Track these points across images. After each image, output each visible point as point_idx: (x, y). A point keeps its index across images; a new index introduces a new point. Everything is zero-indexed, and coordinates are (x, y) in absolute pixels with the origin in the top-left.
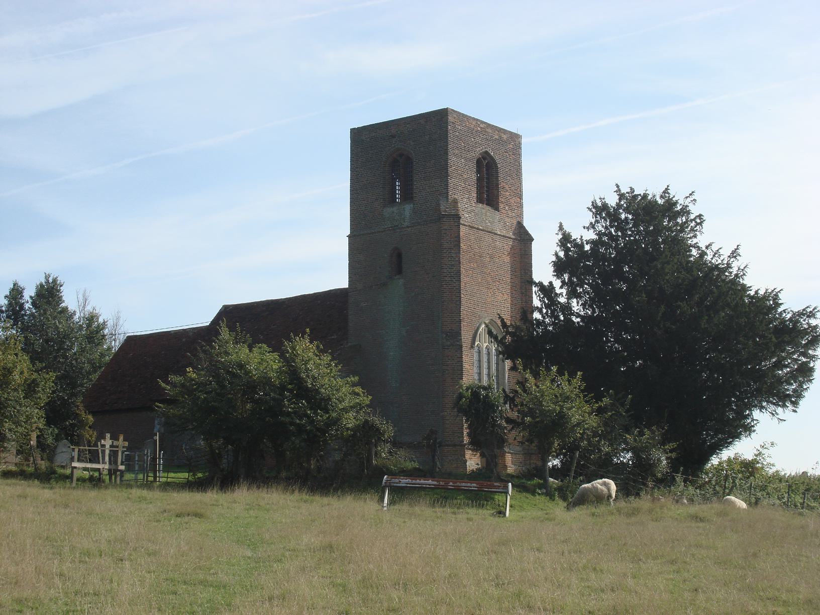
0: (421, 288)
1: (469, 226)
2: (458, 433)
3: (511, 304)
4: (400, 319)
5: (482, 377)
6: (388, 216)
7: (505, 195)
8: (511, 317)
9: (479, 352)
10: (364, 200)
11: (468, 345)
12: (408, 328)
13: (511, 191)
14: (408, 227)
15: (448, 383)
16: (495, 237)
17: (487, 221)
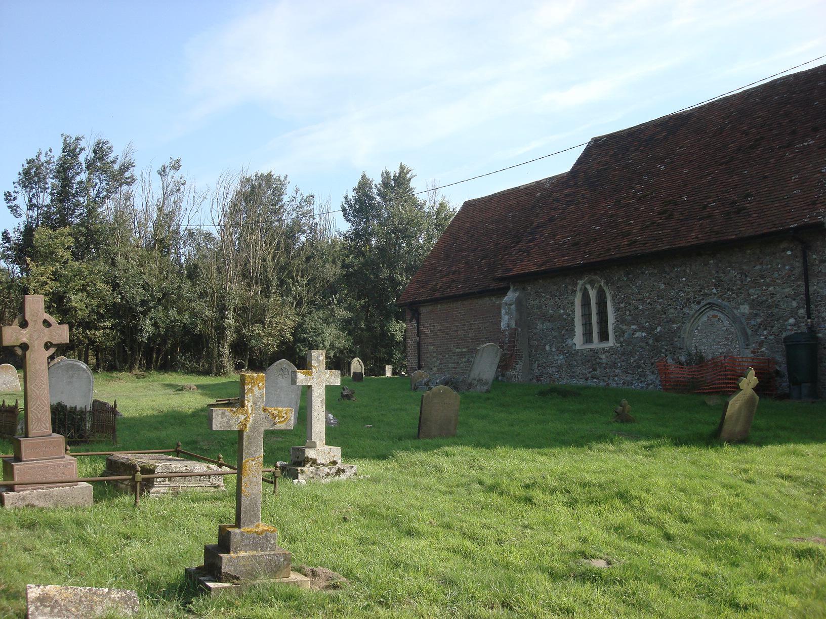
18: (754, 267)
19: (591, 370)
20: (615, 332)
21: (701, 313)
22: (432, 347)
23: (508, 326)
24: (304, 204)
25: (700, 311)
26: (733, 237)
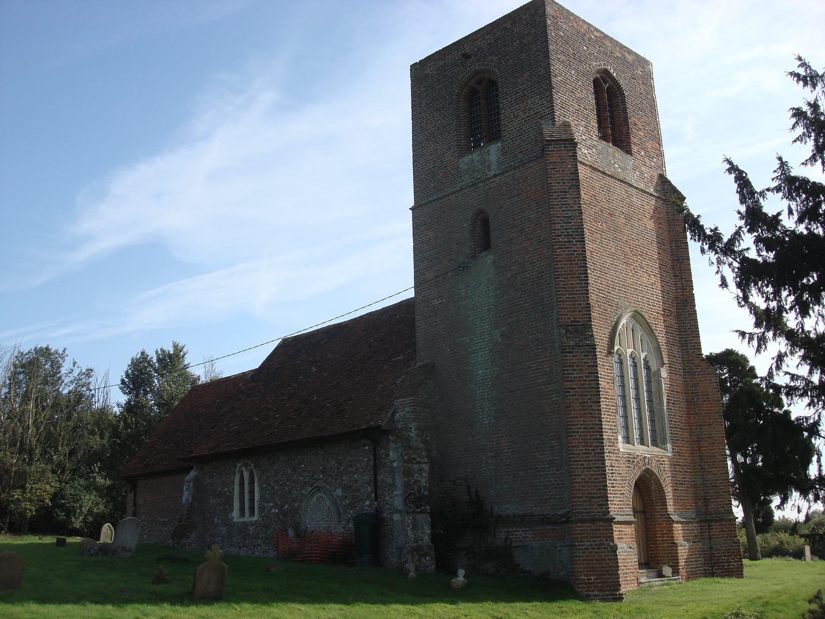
0: (520, 264)
1: (591, 166)
2: (599, 497)
3: (661, 291)
4: (490, 316)
5: (628, 403)
6: (466, 168)
7: (637, 136)
8: (664, 310)
9: (621, 362)
10: (431, 154)
11: (603, 349)
12: (504, 329)
13: (645, 132)
14: (495, 176)
15: (575, 410)
16: (630, 189)
17: (616, 166)
18: (346, 458)
19: (243, 540)
20: (259, 508)
21: (312, 494)
22: (144, 517)
23: (187, 501)
24: (83, 377)
25: (312, 493)
26: (328, 434)
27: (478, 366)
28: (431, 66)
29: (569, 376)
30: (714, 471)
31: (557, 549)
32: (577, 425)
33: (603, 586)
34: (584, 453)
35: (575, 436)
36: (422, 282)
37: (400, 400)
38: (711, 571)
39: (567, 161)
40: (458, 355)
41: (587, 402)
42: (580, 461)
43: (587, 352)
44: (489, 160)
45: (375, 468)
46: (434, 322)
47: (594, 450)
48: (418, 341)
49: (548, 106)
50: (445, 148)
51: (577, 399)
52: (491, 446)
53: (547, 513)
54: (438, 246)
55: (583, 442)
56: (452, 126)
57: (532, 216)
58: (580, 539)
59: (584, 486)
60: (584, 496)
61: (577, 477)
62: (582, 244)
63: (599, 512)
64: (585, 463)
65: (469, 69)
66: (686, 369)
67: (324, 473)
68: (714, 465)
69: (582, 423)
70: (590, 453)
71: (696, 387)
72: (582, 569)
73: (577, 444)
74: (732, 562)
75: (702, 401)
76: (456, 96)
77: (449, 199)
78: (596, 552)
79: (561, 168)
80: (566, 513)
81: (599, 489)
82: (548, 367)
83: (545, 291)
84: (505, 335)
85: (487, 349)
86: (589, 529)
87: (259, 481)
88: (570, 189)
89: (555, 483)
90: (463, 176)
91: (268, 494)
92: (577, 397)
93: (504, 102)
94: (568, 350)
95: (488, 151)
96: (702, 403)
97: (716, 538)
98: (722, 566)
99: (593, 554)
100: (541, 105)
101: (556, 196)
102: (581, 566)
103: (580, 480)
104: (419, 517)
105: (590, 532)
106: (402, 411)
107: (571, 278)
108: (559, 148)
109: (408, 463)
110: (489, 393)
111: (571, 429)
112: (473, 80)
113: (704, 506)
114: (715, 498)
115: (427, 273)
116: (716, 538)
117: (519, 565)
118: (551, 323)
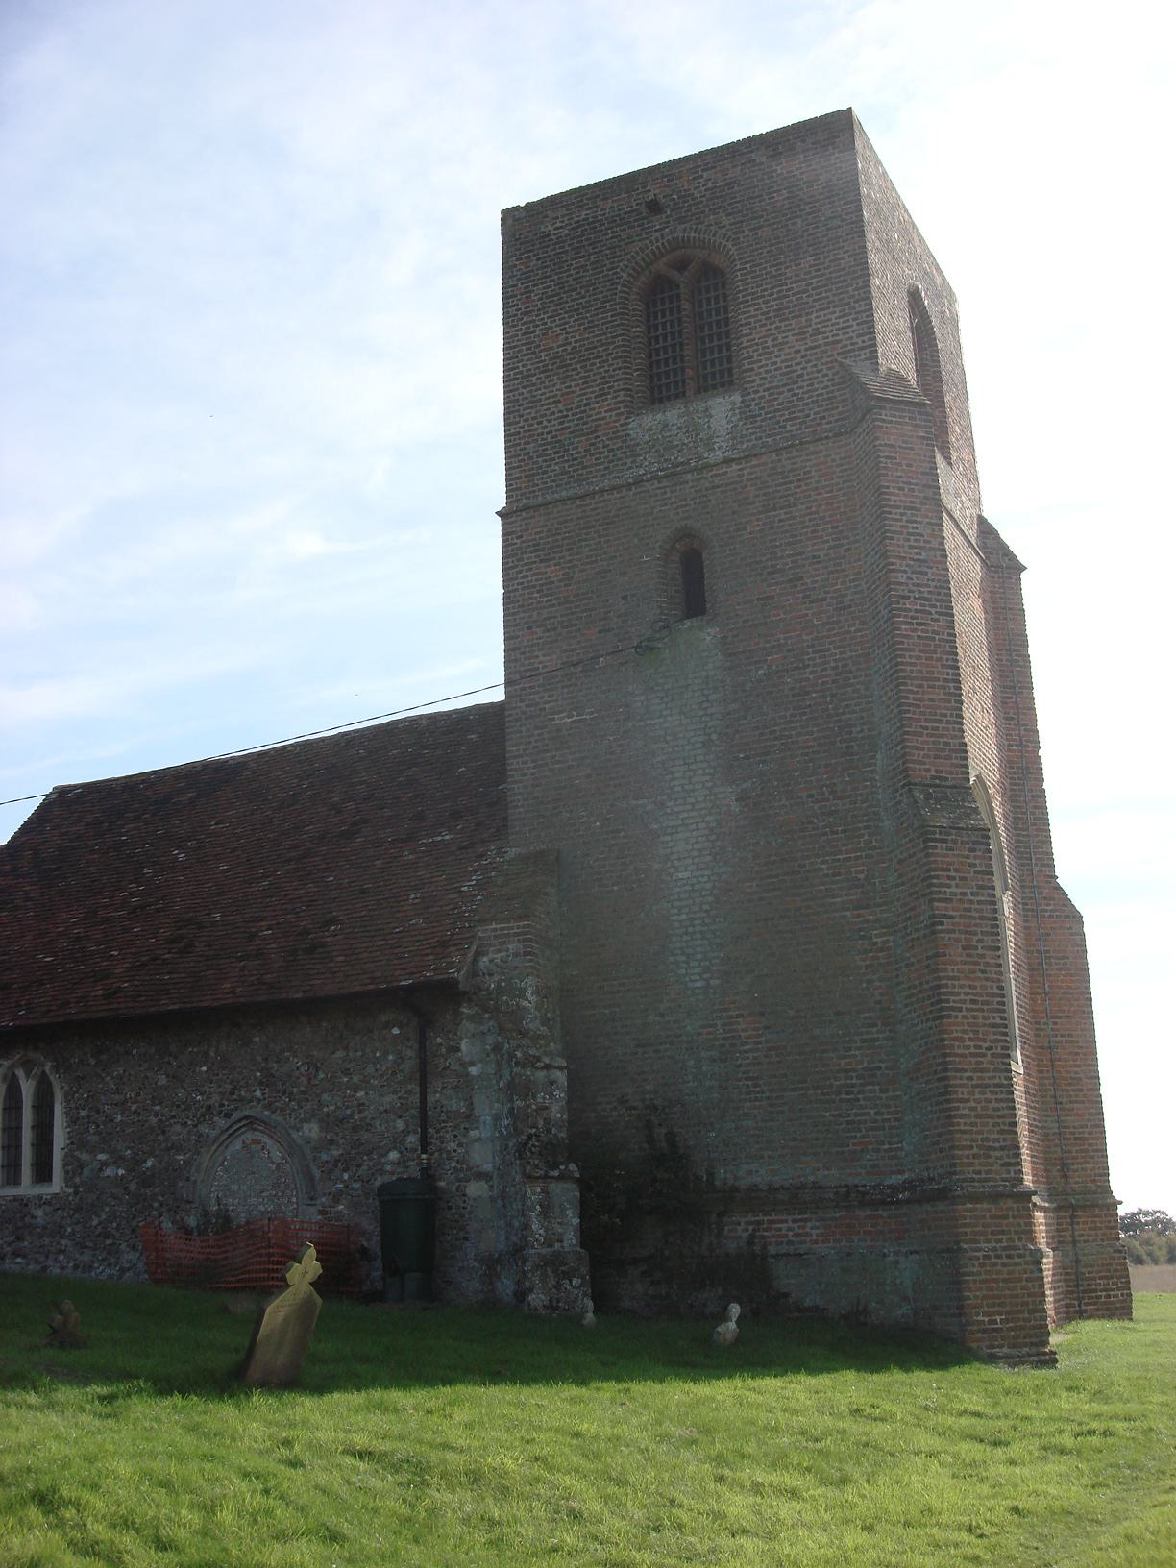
2: (1002, 1149)
6: (647, 438)
10: (555, 402)
14: (728, 461)
18: (333, 1053)
19: (12, 1238)
21: (230, 1135)
27: (676, 863)
28: (557, 218)
29: (943, 889)
30: (1078, 1109)
31: (887, 1259)
32: (959, 993)
33: (1018, 1337)
34: (972, 1055)
35: (956, 1017)
36: (528, 674)
37: (494, 926)
38: (1078, 1308)
39: (915, 447)
40: (624, 837)
41: (976, 948)
42: (966, 1071)
43: (974, 843)
44: (709, 427)
45: (424, 1076)
46: (558, 762)
47: (991, 1048)
48: (511, 802)
49: (861, 332)
50: (592, 393)
51: (958, 940)
52: (711, 1036)
53: (856, 1181)
54: (571, 598)
55: (972, 1031)
56: (611, 347)
57: (821, 554)
58: (972, 1237)
59: (975, 1124)
60: (974, 1144)
61: (961, 1105)
62: (948, 621)
63: (1003, 1180)
64: (975, 1075)
65: (657, 234)
66: (1027, 904)
67: (267, 1085)
68: (1077, 1096)
69: (967, 989)
70: (984, 1055)
71: (1046, 940)
72: (979, 1301)
73: (960, 1035)
74: (1113, 1290)
75: (1057, 969)
76: (624, 286)
77: (604, 501)
78: (1004, 1265)
79: (905, 459)
80: (904, 1182)
81: (1002, 1132)
82: (862, 872)
83: (854, 712)
84: (749, 798)
85: (703, 825)
86: (988, 1214)
87: (68, 1101)
88: (923, 504)
89: (879, 1118)
90: (640, 455)
91: (94, 1134)
92: (956, 935)
93: (750, 312)
94: (937, 836)
95: (707, 410)
96: (1056, 972)
97: (1085, 1242)
98: (1097, 1297)
99: (1000, 1268)
100: (843, 328)
101: (896, 514)
102: (978, 1293)
103: (966, 1111)
104: (554, 1187)
105: (989, 1221)
106: (499, 951)
107: (929, 687)
108: (900, 417)
109: (524, 1066)
110: (707, 921)
111: (948, 1001)
112: (664, 259)
113: (1062, 1177)
114: (1081, 1163)
115: (540, 654)
116: (1085, 1242)
117: (786, 1296)
118: (871, 780)
